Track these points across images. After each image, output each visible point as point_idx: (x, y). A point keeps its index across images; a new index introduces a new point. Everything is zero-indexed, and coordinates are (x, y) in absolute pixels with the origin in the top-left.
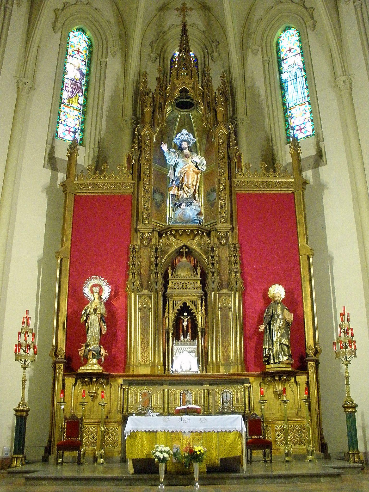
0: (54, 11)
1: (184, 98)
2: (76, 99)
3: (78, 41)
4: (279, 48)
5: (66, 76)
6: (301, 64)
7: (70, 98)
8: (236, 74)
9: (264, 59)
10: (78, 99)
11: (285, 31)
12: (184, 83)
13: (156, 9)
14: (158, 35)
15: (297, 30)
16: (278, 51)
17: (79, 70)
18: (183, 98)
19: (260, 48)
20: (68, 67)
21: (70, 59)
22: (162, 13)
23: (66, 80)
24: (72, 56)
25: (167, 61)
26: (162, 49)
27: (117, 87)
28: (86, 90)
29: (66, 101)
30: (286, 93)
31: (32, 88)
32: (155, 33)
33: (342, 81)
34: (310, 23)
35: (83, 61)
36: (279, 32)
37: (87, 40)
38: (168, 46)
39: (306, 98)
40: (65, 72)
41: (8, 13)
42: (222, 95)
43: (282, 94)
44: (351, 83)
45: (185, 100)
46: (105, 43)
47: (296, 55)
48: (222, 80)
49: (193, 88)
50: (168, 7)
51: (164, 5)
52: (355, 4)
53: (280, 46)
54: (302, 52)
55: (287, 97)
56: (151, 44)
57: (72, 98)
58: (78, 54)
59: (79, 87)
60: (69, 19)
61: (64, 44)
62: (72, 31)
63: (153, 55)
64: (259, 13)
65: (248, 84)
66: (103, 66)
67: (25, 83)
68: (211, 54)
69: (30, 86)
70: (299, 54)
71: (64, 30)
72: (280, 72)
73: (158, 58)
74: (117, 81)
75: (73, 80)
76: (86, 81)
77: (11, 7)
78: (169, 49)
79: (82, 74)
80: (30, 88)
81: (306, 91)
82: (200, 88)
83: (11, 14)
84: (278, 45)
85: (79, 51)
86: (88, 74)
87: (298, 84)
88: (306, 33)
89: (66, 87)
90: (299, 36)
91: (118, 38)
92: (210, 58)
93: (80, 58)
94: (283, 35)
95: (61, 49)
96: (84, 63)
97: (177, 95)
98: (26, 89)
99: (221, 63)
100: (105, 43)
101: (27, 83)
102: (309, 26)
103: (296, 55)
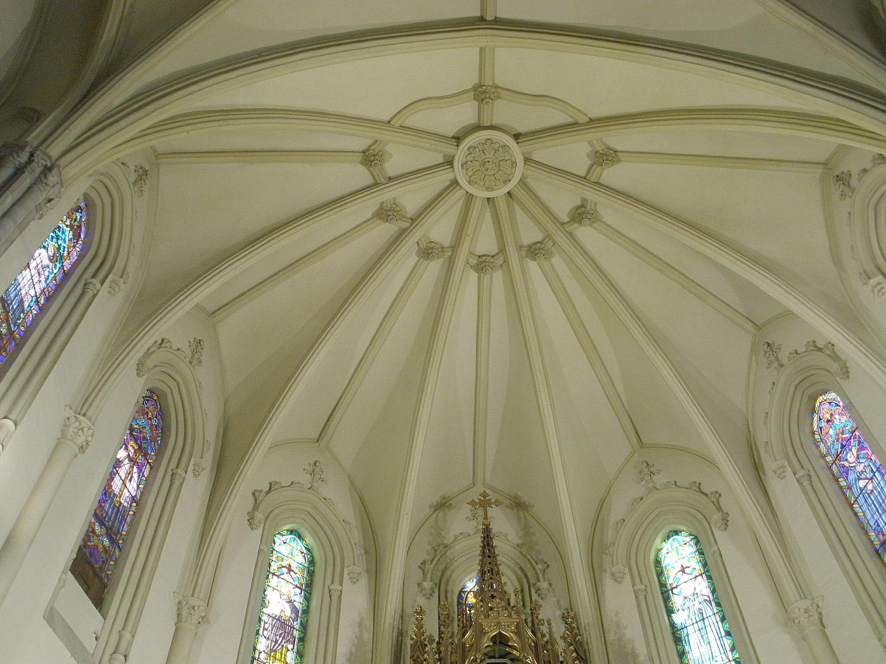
0: (253, 494)
1: (497, 655)
2: (281, 654)
3: (290, 551)
4: (662, 568)
5: (265, 610)
6: (707, 592)
7: (271, 650)
8: (586, 615)
9: (636, 588)
10: (285, 655)
11: (668, 537)
12: (498, 624)
13: (430, 506)
14: (436, 551)
15: (690, 535)
16: (660, 574)
17: (290, 602)
18: (494, 657)
19: (627, 569)
20: (270, 594)
21: (273, 581)
22: (441, 515)
23: (265, 618)
24: (278, 576)
25: (452, 597)
26: (443, 574)
27: (359, 638)
28: (301, 640)
29: (263, 656)
30: (687, 648)
31: (204, 620)
32: (429, 548)
33: (802, 611)
34: (716, 517)
35: (297, 586)
36: (658, 540)
37: (305, 551)
38: (453, 571)
39: (730, 653)
40: (263, 603)
41: (177, 483)
42: (572, 648)
43: (678, 651)
44: (820, 613)
45: (497, 661)
46: (338, 559)
47: (696, 577)
48: (566, 623)
49: (518, 633)
50: (451, 505)
51: (444, 501)
52: (798, 476)
53: (664, 565)
54: (708, 571)
55: (690, 656)
56: (423, 566)
57: (275, 651)
58: (289, 573)
59: (289, 634)
60: (277, 511)
61: (266, 550)
62: (279, 533)
63: (427, 585)
64: (617, 510)
65: (611, 637)
66: (335, 600)
67: (193, 608)
68: (534, 585)
69: (203, 614)
70: (701, 575)
71: (268, 524)
72: (670, 612)
73: (436, 590)
74: (359, 627)
75: (278, 620)
76: (301, 623)
77: (183, 474)
78: (454, 576)
79: (294, 610)
80: (203, 617)
81: (727, 642)
82: (530, 634)
83: (181, 484)
84: (658, 562)
85: (290, 569)
86: (306, 612)
87: (708, 628)
88: (710, 535)
89: (264, 629)
90: (696, 544)
91: (363, 552)
92: (533, 591)
93: (291, 581)
94: (667, 546)
95: (261, 558)
96: (298, 591)
97: (486, 642)
98: (195, 619)
99: (554, 599)
100: (338, 559)
101: (196, 608)
102: (716, 523)
103: (696, 577)
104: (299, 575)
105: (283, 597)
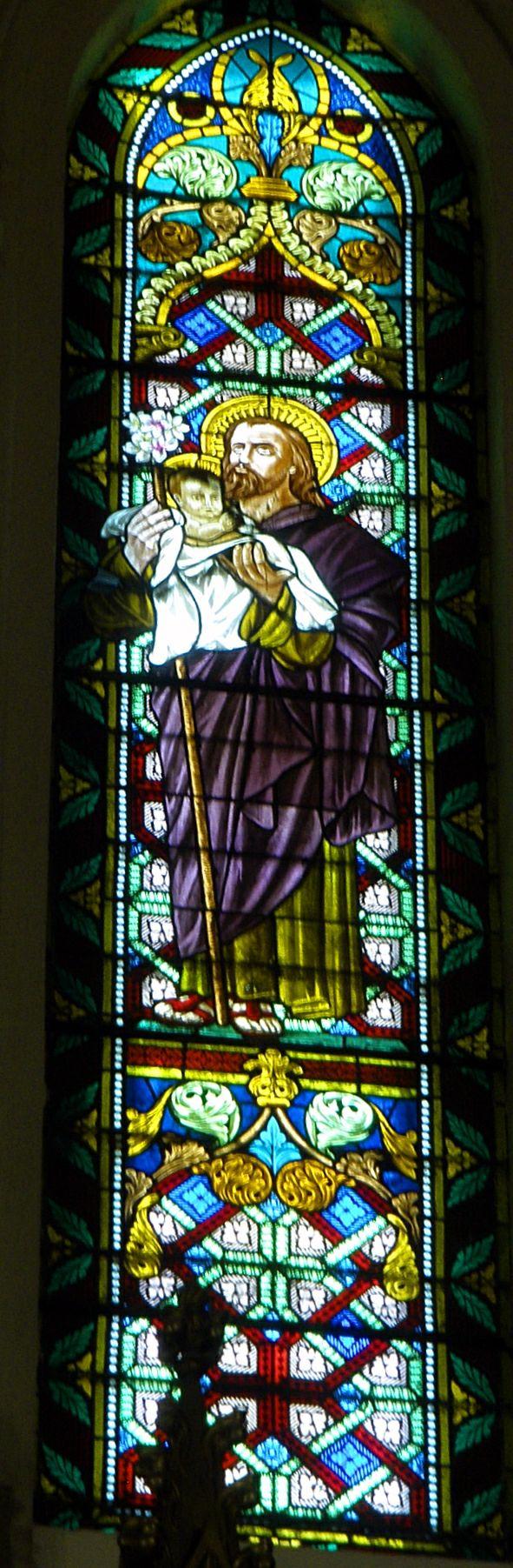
1: (166, 513)
2: (315, 919)
20: (165, 535)
23: (137, 710)
24: (184, 374)
35: (351, 391)
76: (442, 651)
85: (269, 282)
86: (459, 548)
93: (303, 362)
104: (358, 296)
105: (259, 508)
